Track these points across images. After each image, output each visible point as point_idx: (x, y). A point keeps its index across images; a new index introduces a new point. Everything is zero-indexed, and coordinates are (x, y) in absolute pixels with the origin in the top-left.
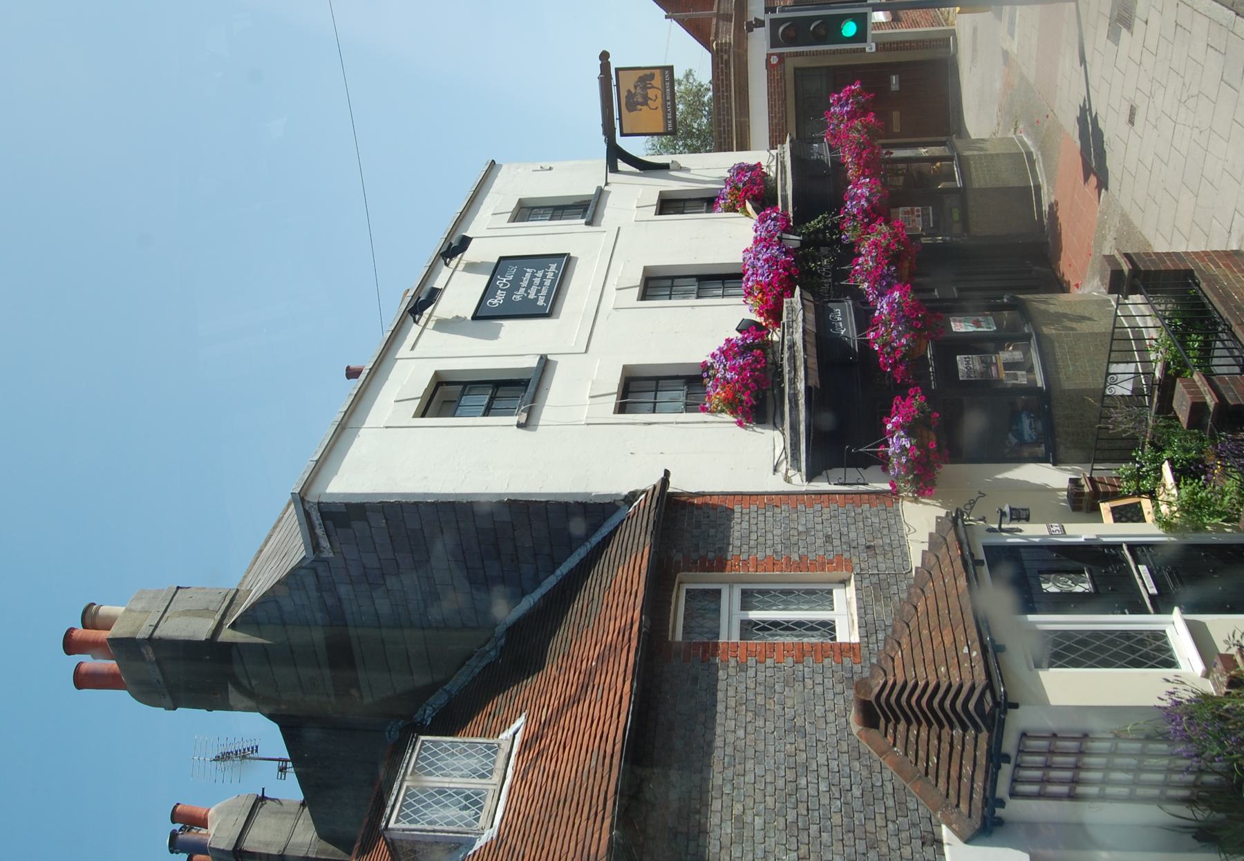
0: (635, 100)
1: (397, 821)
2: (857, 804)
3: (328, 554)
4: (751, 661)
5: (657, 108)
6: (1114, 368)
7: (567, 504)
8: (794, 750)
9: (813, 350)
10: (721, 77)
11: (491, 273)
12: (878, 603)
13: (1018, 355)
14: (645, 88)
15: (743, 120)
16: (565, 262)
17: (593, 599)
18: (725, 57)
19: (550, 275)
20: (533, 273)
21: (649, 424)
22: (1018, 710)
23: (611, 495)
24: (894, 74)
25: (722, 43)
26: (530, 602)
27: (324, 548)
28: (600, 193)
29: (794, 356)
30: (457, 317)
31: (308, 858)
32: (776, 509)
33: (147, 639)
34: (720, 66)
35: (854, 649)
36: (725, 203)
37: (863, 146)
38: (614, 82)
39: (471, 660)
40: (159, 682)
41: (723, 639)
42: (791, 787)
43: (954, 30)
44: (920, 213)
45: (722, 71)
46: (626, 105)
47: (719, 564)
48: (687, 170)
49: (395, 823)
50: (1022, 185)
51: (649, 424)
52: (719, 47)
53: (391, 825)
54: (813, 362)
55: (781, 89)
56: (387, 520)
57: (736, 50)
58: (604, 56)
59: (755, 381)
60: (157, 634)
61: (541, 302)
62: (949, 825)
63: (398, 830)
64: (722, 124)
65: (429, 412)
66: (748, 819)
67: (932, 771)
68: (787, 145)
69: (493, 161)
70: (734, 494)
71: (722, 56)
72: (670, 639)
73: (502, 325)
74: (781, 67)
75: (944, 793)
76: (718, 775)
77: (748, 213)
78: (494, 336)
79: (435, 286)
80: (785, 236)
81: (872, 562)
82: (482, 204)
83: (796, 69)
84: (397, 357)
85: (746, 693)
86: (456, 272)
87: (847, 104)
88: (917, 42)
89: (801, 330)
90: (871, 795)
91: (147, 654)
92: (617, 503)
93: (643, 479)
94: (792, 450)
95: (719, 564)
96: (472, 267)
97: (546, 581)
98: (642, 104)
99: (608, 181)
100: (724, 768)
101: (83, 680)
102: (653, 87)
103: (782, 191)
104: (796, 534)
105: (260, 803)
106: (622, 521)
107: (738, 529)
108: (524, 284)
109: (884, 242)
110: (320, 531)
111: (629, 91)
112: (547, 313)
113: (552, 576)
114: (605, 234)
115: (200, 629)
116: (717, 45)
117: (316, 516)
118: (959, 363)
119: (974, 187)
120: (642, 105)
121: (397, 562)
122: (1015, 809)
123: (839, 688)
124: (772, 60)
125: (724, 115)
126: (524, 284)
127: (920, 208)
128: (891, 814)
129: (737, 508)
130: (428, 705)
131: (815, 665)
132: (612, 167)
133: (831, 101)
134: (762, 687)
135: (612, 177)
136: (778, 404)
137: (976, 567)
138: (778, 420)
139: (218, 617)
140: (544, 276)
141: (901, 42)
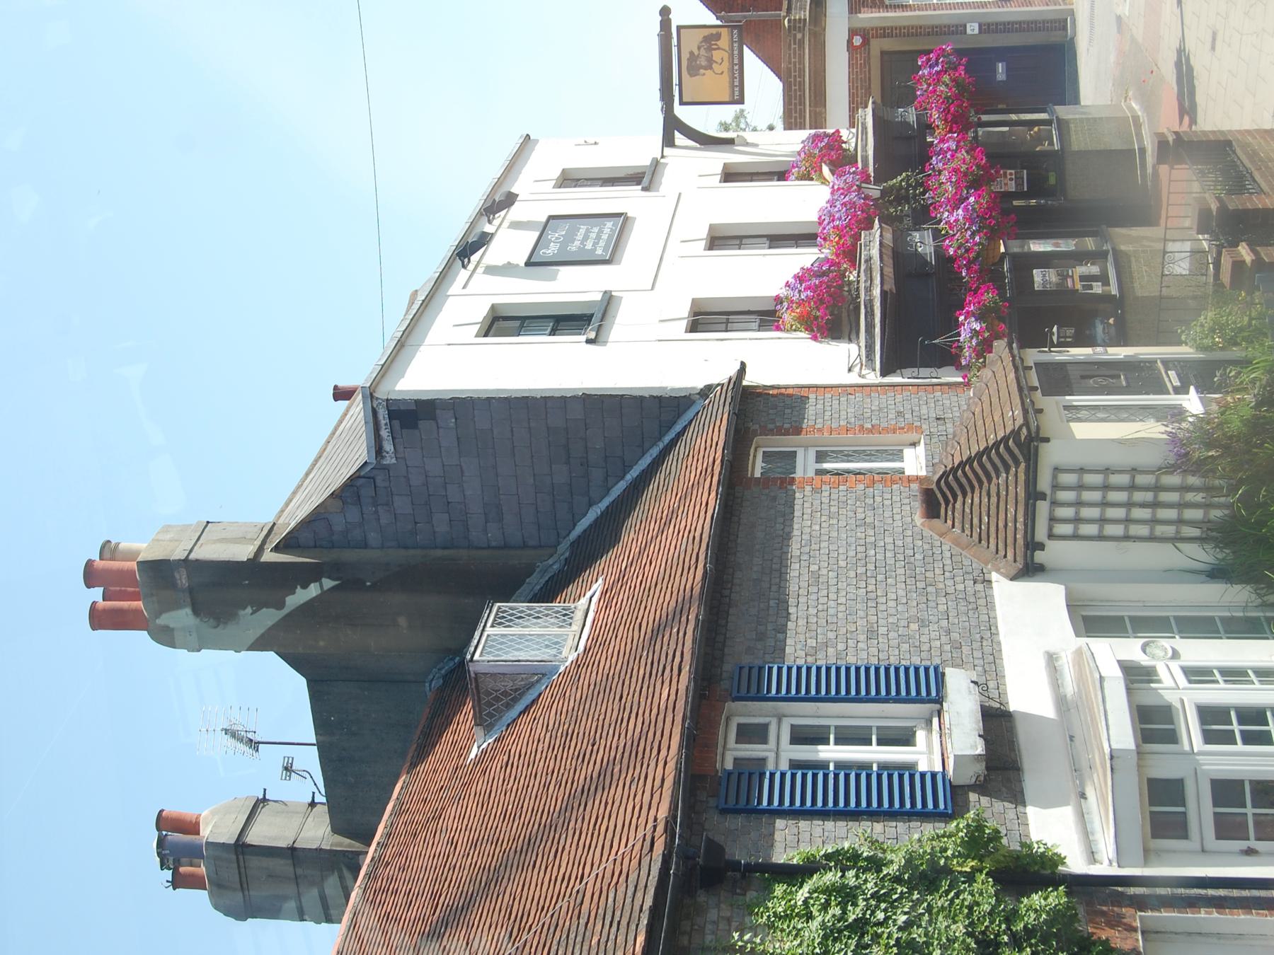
1: (481, 655)
3: (389, 460)
5: (722, 73)
6: (1171, 247)
7: (642, 398)
9: (889, 261)
10: (793, 60)
11: (541, 229)
13: (1094, 270)
14: (710, 49)
15: (818, 109)
16: (623, 221)
17: (670, 473)
18: (799, 36)
19: (607, 230)
20: (587, 229)
21: (722, 340)
22: (1050, 444)
23: (686, 388)
24: (1000, 61)
25: (795, 20)
27: (387, 453)
28: (656, 165)
29: (871, 268)
30: (509, 263)
31: (321, 849)
32: (850, 396)
33: (183, 560)
34: (793, 46)
36: (799, 171)
37: (951, 101)
38: (675, 41)
39: (532, 577)
41: (799, 474)
43: (1073, 10)
44: (1013, 177)
45: (795, 54)
47: (797, 431)
48: (755, 145)
49: (480, 656)
50: (1125, 147)
51: (722, 340)
52: (792, 24)
53: (476, 657)
54: (889, 270)
55: (865, 75)
56: (456, 419)
57: (812, 28)
58: (665, 12)
59: (831, 296)
60: (192, 556)
61: (599, 252)
62: (998, 571)
63: (483, 661)
64: (794, 115)
65: (491, 333)
67: (984, 536)
68: (869, 110)
69: (528, 135)
70: (809, 387)
71: (795, 35)
73: (558, 270)
74: (865, 49)
75: (994, 550)
77: (825, 179)
78: (553, 278)
79: (512, 191)
80: (864, 185)
81: (940, 428)
82: (520, 173)
83: (883, 53)
84: (448, 293)
86: (475, 275)
87: (937, 64)
88: (1028, 23)
89: (878, 243)
91: (181, 579)
92: (692, 397)
93: (721, 373)
94: (867, 351)
95: (797, 431)
96: (516, 225)
97: (614, 489)
99: (665, 154)
102: (719, 49)
103: (862, 151)
105: (262, 805)
106: (698, 413)
107: (810, 411)
109: (964, 168)
110: (384, 433)
111: (692, 53)
113: (622, 482)
115: (243, 553)
116: (789, 21)
117: (383, 414)
118: (1035, 276)
119: (1073, 149)
120: (706, 69)
121: (461, 468)
122: (1053, 553)
123: (907, 501)
124: (854, 41)
127: (1013, 171)
129: (812, 396)
132: (668, 141)
133: (920, 63)
135: (667, 151)
136: (854, 325)
137: (1021, 350)
138: (853, 336)
139: (258, 543)
141: (1009, 23)
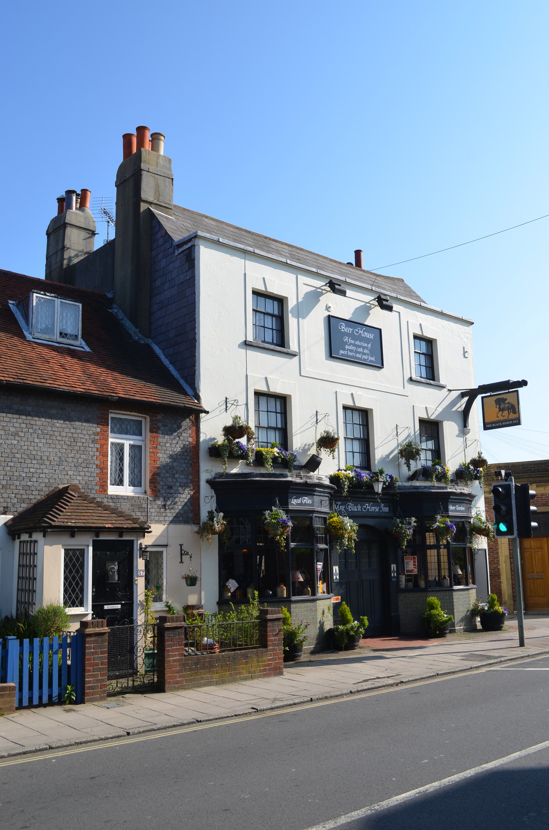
0: (502, 404)
1: (37, 297)
2: (24, 483)
4: (98, 446)
5: (498, 417)
8: (51, 460)
12: (130, 505)
14: (508, 409)
26: (160, 353)
35: (105, 491)
40: (125, 177)
42: (32, 457)
46: (499, 398)
49: (36, 296)
56: (189, 279)
60: (144, 174)
66: (17, 438)
72: (110, 411)
76: (38, 427)
85: (80, 442)
90: (27, 488)
98: (499, 408)
100: (42, 430)
101: (127, 138)
102: (509, 414)
104: (173, 473)
108: (358, 343)
111: (506, 399)
112: (332, 354)
113: (169, 363)
114: (403, 389)
117: (189, 245)
125: (535, 467)
126: (358, 343)
128: (19, 496)
130: (119, 310)
131: (95, 473)
134: (83, 449)
139: (155, 202)
140: (365, 354)
